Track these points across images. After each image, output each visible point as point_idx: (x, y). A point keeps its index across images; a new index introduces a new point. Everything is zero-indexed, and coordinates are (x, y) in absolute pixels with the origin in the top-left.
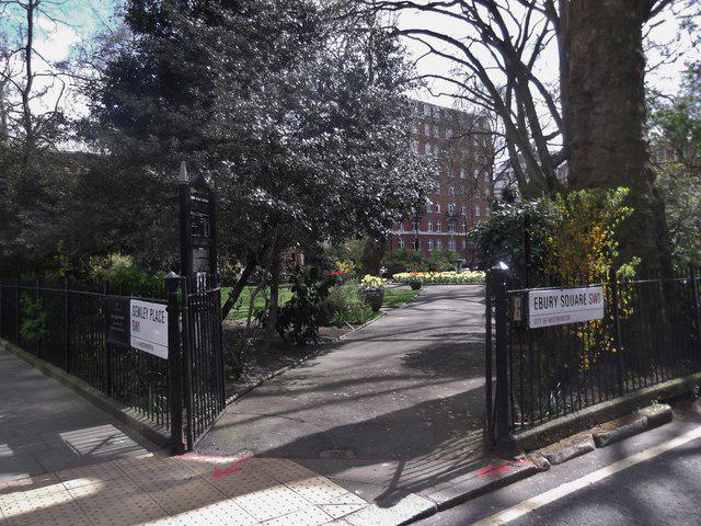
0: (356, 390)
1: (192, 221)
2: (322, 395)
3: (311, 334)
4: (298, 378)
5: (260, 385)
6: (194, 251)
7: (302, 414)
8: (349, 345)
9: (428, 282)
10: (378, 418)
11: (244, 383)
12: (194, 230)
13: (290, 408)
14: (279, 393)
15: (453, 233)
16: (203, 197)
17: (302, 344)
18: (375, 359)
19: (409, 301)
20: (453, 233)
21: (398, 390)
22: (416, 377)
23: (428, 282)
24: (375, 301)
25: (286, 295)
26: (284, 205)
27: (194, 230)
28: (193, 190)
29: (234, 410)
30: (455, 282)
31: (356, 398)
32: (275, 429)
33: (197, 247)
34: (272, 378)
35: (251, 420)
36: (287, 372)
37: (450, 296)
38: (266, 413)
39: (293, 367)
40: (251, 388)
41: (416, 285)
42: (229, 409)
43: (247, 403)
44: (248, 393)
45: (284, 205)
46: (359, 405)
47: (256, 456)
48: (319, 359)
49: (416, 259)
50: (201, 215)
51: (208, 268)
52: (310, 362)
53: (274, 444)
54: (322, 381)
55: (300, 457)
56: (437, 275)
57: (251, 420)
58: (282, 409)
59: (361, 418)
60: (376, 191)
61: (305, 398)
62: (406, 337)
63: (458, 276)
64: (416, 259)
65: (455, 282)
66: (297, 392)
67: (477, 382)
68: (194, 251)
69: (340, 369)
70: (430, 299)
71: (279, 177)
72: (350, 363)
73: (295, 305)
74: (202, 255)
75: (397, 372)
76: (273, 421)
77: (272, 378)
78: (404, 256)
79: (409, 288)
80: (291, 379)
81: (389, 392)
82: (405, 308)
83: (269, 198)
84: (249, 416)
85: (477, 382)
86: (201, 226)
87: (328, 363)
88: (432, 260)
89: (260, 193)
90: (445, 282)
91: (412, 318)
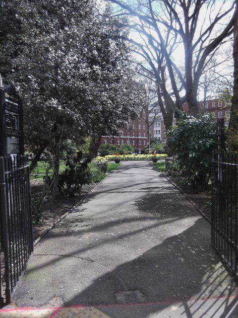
0: (119, 230)
1: (6, 117)
2: (98, 235)
3: (78, 190)
4: (77, 220)
5: (53, 227)
6: (8, 138)
7: (89, 254)
8: (98, 196)
9: (123, 160)
10: (144, 254)
11: (42, 225)
12: (8, 124)
13: (79, 248)
14: (68, 234)
15: (129, 137)
16: (14, 101)
17: (72, 196)
18: (119, 205)
19: (118, 169)
20: (129, 137)
21: (145, 229)
22: (151, 219)
23: (123, 160)
24: (104, 168)
25: (63, 168)
26: (69, 111)
27: (8, 124)
28: (7, 95)
29: (42, 251)
30: (135, 159)
31: (121, 237)
32: (74, 271)
33: (10, 136)
34: (60, 221)
35: (53, 262)
36: (69, 216)
37: (136, 166)
38: (63, 253)
39: (71, 212)
40: (48, 231)
41: (117, 161)
42: (36, 250)
43: (49, 243)
44: (47, 235)
45: (69, 111)
46: (126, 243)
47: (67, 305)
48: (84, 206)
49: (113, 149)
50: (13, 114)
51: (18, 151)
52: (79, 208)
53: (77, 288)
54: (94, 223)
55: (103, 303)
56: (126, 156)
57: (53, 262)
58: (73, 249)
59: (133, 256)
60: (117, 107)
61: (87, 238)
62: (128, 189)
63: (136, 156)
64: (113, 149)
65: (135, 159)
66: (80, 233)
67: (188, 222)
68: (8, 138)
69: (100, 213)
70: (127, 168)
71: (69, 95)
72: (105, 208)
73: (68, 174)
74: (13, 142)
75: (137, 214)
76: (70, 262)
77: (60, 221)
78: (108, 147)
79: (114, 162)
80: (73, 222)
81: (140, 231)
82: (117, 172)
83: (59, 105)
84: (52, 257)
85: (188, 222)
86: (13, 122)
87: (92, 208)
88: (120, 149)
89: (54, 102)
90: (131, 159)
91: (123, 178)
